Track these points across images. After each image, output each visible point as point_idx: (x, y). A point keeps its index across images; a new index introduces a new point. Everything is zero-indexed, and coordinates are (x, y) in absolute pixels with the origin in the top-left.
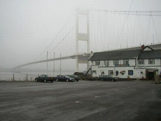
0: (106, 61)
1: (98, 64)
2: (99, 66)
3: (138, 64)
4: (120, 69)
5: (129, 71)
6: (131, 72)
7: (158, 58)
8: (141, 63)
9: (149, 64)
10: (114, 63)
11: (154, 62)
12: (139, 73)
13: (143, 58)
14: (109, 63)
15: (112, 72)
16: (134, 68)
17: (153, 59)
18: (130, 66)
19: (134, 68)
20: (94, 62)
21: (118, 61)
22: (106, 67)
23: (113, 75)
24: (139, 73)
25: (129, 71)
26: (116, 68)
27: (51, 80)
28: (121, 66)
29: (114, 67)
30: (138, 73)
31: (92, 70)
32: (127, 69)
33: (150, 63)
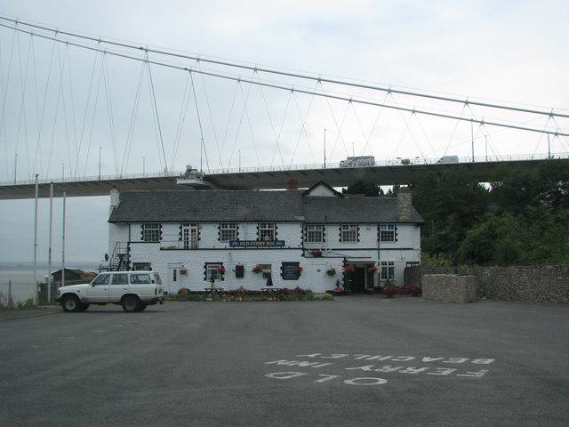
0: (190, 228)
1: (152, 236)
2: (163, 244)
3: (219, 240)
4: (250, 259)
5: (284, 264)
6: (291, 270)
7: (370, 223)
8: (315, 238)
9: (340, 241)
10: (219, 234)
11: (238, 234)
12: (319, 271)
13: (324, 221)
14: (199, 233)
15: (215, 272)
16: (303, 255)
17: (353, 224)
18: (289, 248)
19: (303, 255)
20: (137, 231)
21: (238, 228)
22: (186, 248)
23: (223, 279)
24: (319, 271)
25: (284, 264)
26: (232, 251)
27: (104, 304)
28: (248, 246)
29: (225, 249)
30: (318, 268)
31: (134, 259)
32: (275, 259)
33: (346, 237)
